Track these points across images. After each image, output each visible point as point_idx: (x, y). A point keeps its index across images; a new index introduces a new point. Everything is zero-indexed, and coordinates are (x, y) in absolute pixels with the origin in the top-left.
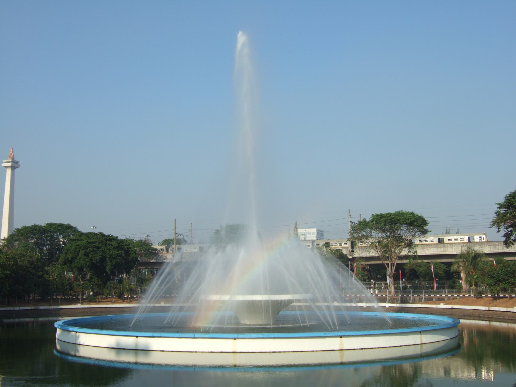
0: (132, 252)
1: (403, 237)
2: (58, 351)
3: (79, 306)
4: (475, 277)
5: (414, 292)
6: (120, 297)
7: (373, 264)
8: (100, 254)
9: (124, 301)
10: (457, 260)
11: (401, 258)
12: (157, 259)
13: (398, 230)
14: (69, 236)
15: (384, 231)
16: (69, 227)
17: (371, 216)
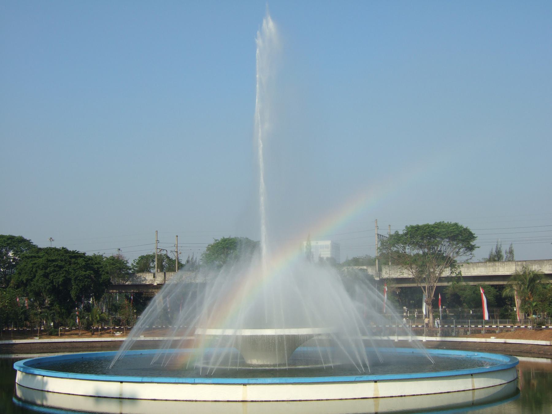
0: (104, 273)
1: (444, 255)
2: (19, 399)
3: (36, 340)
4: (534, 304)
5: (458, 323)
6: (88, 329)
7: (406, 288)
8: (63, 275)
9: (93, 334)
10: (510, 283)
11: (441, 279)
12: (133, 280)
13: (438, 246)
14: (22, 251)
15: (421, 247)
16: (22, 240)
17: (405, 228)
